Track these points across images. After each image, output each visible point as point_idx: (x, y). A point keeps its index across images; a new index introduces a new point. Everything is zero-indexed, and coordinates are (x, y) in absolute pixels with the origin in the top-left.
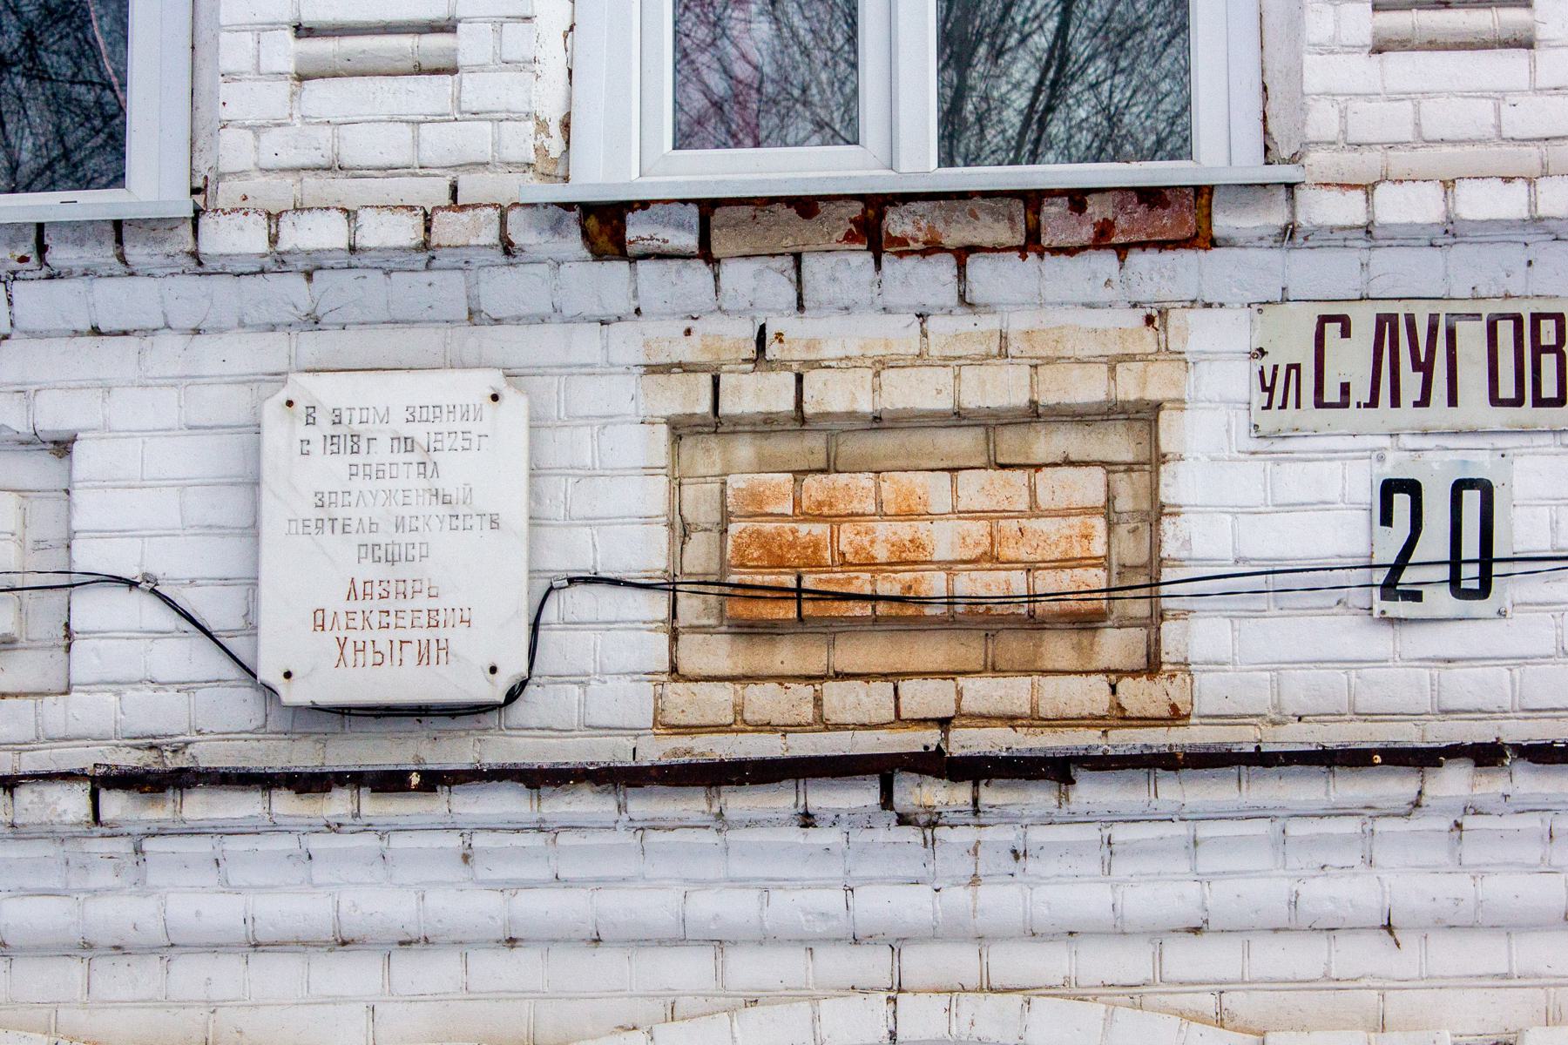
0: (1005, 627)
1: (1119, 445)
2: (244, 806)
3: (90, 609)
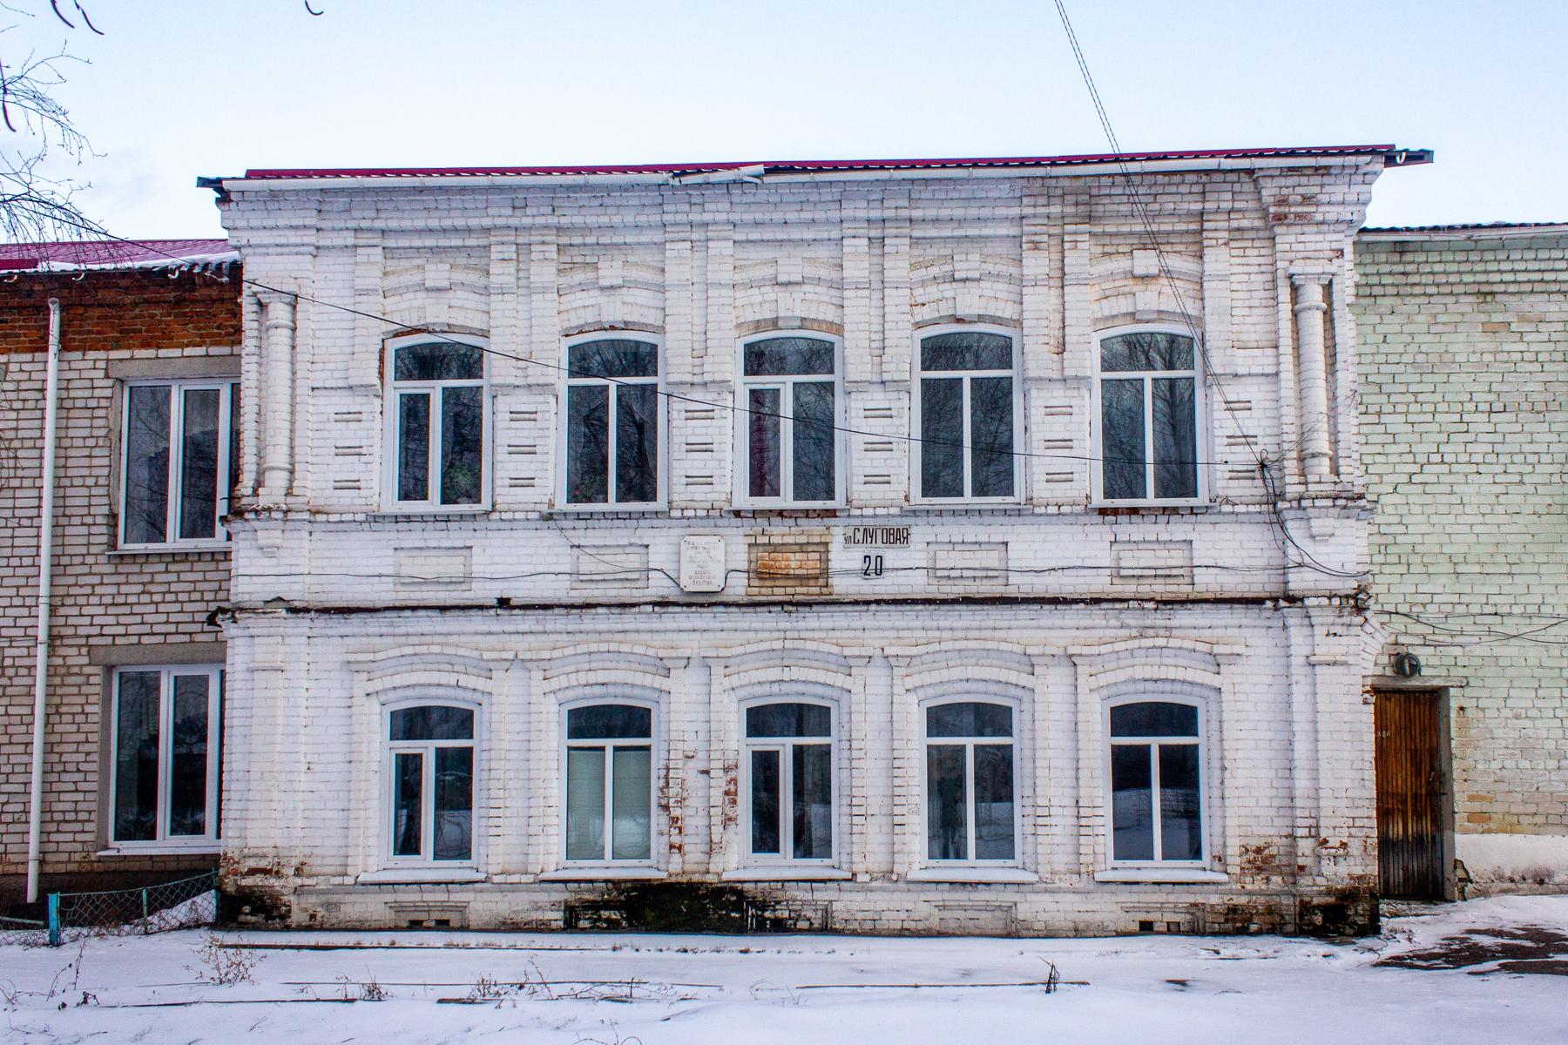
0: (803, 579)
1: (822, 549)
2: (678, 609)
3: (651, 574)
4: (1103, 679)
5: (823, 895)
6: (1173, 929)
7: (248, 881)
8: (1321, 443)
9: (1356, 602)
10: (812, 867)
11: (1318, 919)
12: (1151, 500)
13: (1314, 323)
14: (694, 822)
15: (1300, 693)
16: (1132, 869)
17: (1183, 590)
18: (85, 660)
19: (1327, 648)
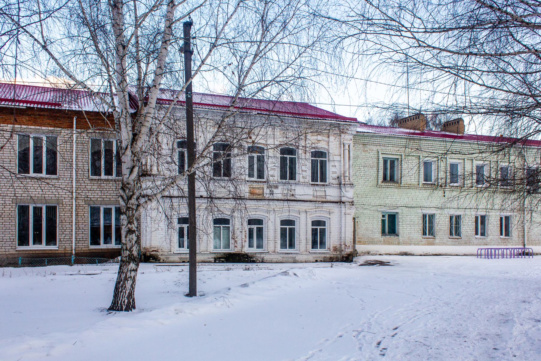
4: (312, 216)
5: (262, 256)
6: (321, 261)
7: (153, 253)
8: (347, 174)
9: (352, 203)
10: (260, 250)
11: (345, 259)
12: (319, 183)
13: (347, 152)
14: (239, 242)
15: (343, 219)
16: (314, 250)
17: (324, 200)
18: (84, 203)
19: (348, 211)
